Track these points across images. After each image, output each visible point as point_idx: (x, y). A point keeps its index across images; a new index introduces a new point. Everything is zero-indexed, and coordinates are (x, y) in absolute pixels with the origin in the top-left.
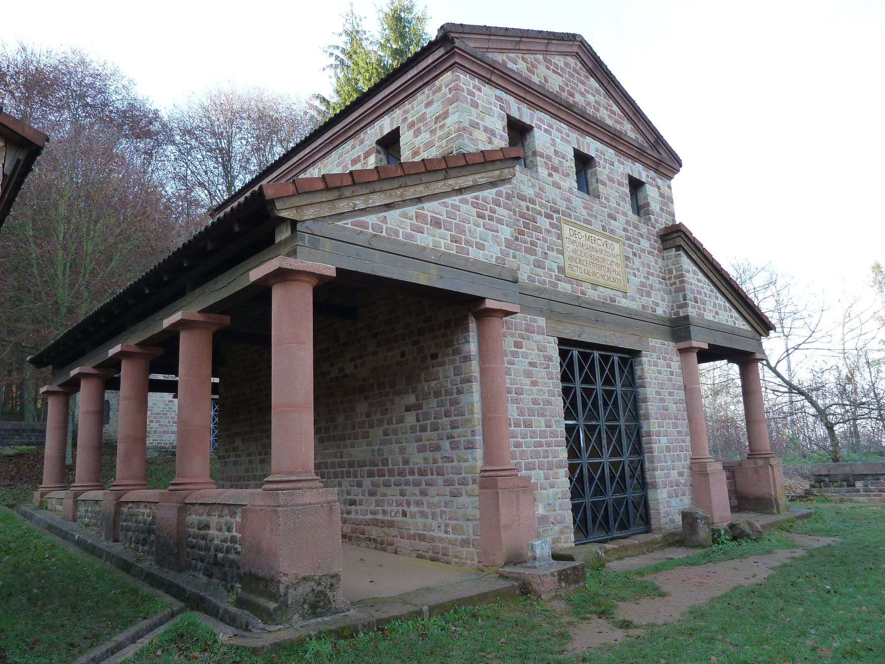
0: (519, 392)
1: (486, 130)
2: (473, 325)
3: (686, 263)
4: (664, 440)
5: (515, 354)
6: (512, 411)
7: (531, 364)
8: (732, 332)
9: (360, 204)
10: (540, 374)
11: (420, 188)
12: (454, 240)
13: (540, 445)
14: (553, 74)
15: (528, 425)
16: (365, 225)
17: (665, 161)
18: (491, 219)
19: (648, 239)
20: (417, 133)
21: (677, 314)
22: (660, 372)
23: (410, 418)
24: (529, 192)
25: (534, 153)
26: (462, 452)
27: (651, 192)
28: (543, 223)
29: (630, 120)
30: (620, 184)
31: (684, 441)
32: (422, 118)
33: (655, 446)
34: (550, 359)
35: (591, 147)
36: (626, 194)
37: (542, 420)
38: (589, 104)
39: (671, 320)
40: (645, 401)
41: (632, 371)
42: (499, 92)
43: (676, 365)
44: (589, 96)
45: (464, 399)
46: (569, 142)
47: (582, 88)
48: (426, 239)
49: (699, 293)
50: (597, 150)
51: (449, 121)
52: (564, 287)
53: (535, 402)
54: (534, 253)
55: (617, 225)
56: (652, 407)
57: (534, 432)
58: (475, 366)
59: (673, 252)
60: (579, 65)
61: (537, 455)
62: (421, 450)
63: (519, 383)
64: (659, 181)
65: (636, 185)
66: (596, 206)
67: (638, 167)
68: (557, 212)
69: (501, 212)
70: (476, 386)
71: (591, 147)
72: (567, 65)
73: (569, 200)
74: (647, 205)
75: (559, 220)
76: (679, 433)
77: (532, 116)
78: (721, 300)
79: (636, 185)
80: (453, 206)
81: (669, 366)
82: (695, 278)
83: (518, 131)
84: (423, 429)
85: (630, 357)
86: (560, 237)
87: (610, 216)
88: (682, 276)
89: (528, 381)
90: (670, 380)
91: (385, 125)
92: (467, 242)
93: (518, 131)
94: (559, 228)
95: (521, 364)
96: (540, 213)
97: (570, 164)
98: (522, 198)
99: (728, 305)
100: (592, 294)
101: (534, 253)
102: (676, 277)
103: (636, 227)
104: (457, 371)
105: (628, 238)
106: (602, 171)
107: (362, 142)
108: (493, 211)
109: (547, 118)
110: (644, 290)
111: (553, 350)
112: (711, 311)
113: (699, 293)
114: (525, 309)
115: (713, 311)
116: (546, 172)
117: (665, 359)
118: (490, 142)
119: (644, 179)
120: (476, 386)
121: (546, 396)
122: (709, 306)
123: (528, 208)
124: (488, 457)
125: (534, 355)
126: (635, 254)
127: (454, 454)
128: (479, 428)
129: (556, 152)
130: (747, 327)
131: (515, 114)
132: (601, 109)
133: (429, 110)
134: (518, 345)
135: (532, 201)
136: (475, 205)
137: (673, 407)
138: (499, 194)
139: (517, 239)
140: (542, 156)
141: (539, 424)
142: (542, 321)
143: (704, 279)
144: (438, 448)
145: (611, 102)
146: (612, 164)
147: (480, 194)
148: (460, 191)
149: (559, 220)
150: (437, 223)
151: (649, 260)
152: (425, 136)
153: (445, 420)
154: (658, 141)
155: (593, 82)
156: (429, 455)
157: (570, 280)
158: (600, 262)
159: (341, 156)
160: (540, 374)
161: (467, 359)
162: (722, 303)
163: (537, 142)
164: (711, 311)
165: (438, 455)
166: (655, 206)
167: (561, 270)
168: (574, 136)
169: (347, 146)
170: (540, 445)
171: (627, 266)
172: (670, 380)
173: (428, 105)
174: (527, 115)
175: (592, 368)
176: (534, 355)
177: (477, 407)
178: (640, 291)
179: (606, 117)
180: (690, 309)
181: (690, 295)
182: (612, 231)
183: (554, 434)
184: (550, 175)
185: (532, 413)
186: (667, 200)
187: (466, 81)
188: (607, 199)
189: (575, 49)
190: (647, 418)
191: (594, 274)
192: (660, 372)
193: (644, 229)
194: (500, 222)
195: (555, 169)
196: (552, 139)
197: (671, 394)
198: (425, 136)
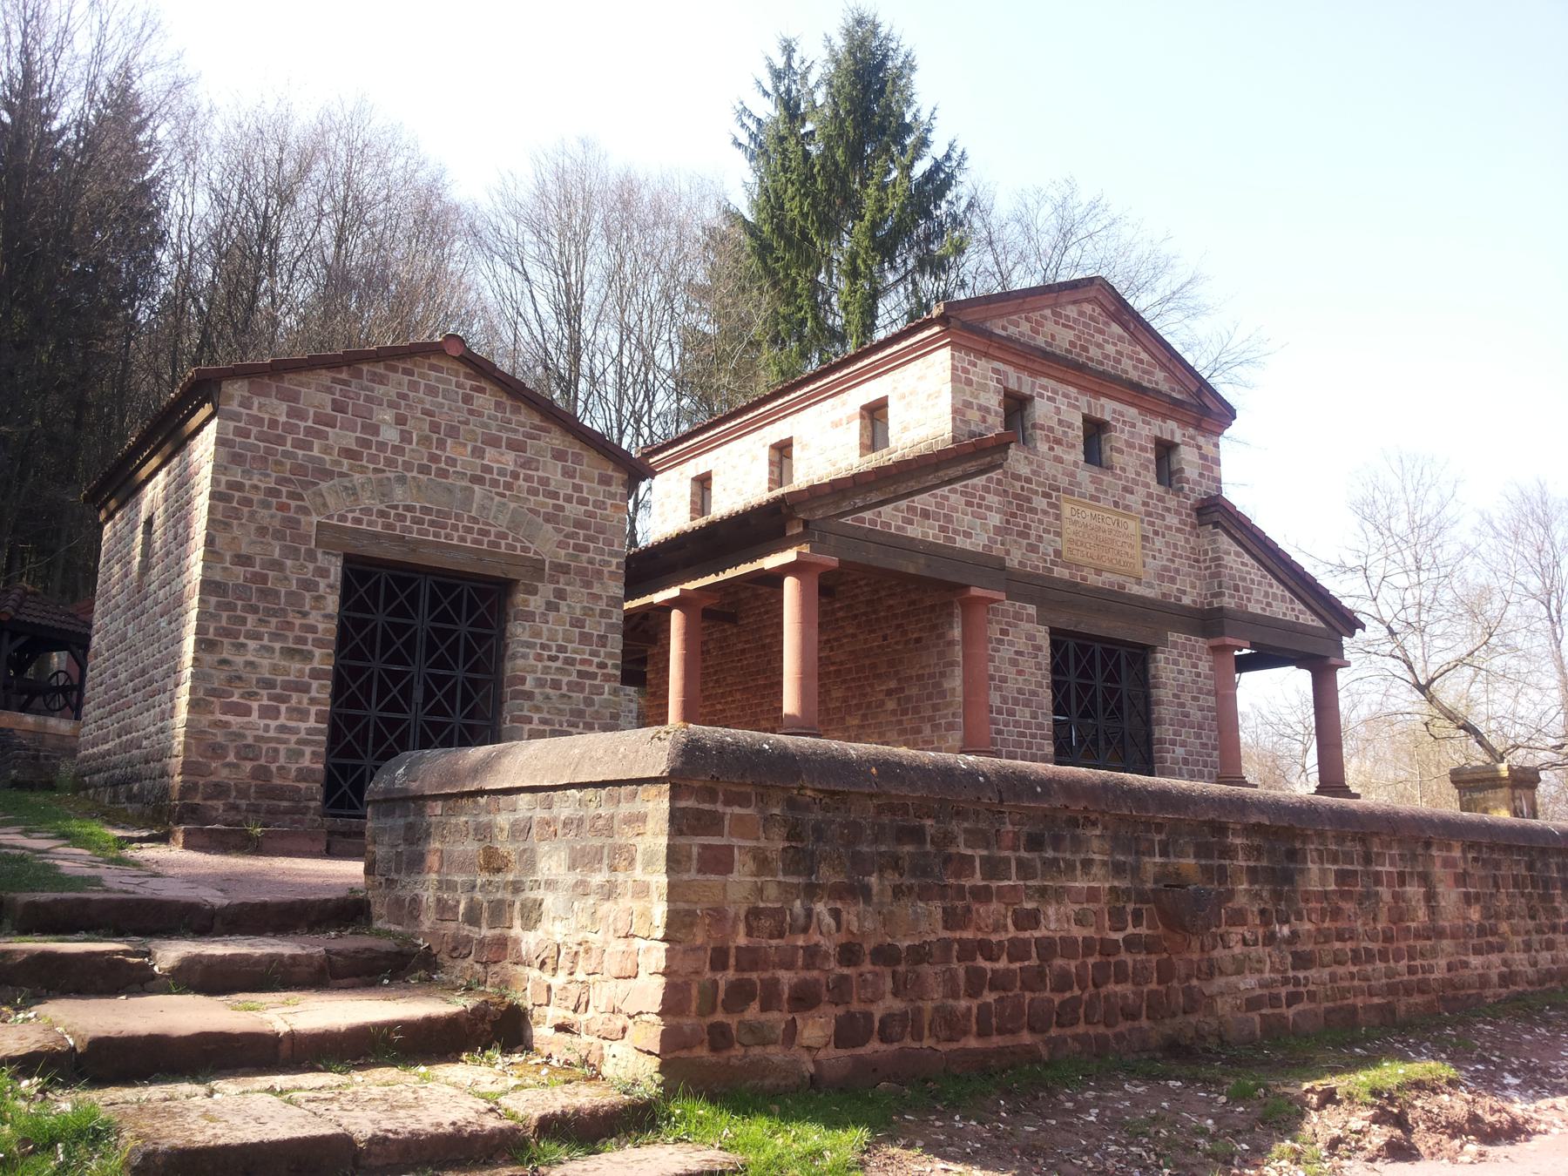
0: (1004, 680)
1: (980, 408)
2: (958, 611)
3: (1225, 542)
4: (1180, 751)
5: (1000, 641)
8: (1292, 628)
10: (1027, 664)
11: (912, 483)
12: (943, 529)
13: (1023, 735)
14: (1057, 334)
15: (1011, 713)
16: (863, 520)
17: (1206, 410)
18: (980, 506)
19: (1178, 513)
21: (1210, 603)
22: (1180, 672)
23: (891, 705)
24: (1025, 470)
27: (1187, 458)
28: (1040, 503)
29: (1163, 367)
31: (1209, 755)
34: (1039, 648)
35: (1107, 409)
36: (1149, 460)
37: (1027, 711)
38: (1107, 357)
41: (1145, 670)
43: (1204, 667)
44: (1110, 348)
46: (1077, 407)
47: (1099, 338)
48: (914, 531)
49: (1244, 579)
50: (1114, 411)
52: (1058, 572)
53: (1020, 691)
54: (1027, 536)
55: (1135, 500)
56: (1165, 711)
57: (1016, 721)
60: (1098, 310)
61: (1019, 744)
63: (1019, 654)
64: (1201, 440)
66: (1107, 478)
67: (1172, 424)
68: (1058, 490)
69: (992, 499)
70: (958, 671)
71: (1107, 409)
72: (1081, 314)
73: (1073, 475)
74: (1181, 470)
75: (1058, 498)
76: (1204, 745)
77: (1033, 384)
78: (1278, 589)
79: (1165, 450)
80: (943, 497)
81: (1195, 666)
82: (1237, 561)
83: (1016, 405)
84: (905, 712)
85: (1141, 655)
86: (1058, 517)
87: (1125, 489)
89: (1014, 670)
90: (1195, 682)
92: (956, 532)
93: (1016, 405)
94: (1056, 506)
95: (1006, 652)
96: (1036, 493)
98: (1017, 477)
99: (1287, 594)
100: (1093, 580)
101: (1027, 536)
102: (1212, 560)
103: (1161, 499)
104: (941, 655)
105: (1149, 514)
106: (1119, 436)
109: (1052, 383)
110: (1163, 575)
112: (1258, 601)
113: (1244, 579)
115: (1269, 600)
117: (1189, 657)
119: (1177, 439)
123: (1022, 488)
125: (1021, 644)
126: (1156, 533)
129: (1060, 422)
130: (1318, 623)
131: (1013, 385)
132: (1124, 360)
134: (1004, 632)
135: (1028, 480)
138: (989, 480)
139: (1008, 522)
140: (1042, 428)
141: (1024, 714)
142: (1032, 609)
145: (1138, 348)
146: (1133, 426)
147: (970, 482)
149: (1058, 498)
150: (926, 514)
154: (1203, 387)
155: (1116, 329)
158: (1110, 538)
160: (1027, 664)
161: (951, 643)
162: (1279, 592)
164: (1258, 601)
166: (1191, 472)
168: (1084, 401)
170: (1023, 735)
171: (1144, 547)
172: (1195, 682)
175: (1091, 660)
176: (1021, 644)
177: (959, 690)
178: (1161, 577)
179: (1130, 369)
180: (1226, 599)
182: (1127, 507)
183: (1040, 726)
184: (1051, 449)
185: (1016, 702)
186: (1211, 463)
188: (1123, 470)
189: (1092, 294)
190: (1160, 722)
192: (1180, 672)
193: (1172, 502)
194: (989, 508)
195: (1058, 442)
196: (1058, 408)
197: (1195, 699)
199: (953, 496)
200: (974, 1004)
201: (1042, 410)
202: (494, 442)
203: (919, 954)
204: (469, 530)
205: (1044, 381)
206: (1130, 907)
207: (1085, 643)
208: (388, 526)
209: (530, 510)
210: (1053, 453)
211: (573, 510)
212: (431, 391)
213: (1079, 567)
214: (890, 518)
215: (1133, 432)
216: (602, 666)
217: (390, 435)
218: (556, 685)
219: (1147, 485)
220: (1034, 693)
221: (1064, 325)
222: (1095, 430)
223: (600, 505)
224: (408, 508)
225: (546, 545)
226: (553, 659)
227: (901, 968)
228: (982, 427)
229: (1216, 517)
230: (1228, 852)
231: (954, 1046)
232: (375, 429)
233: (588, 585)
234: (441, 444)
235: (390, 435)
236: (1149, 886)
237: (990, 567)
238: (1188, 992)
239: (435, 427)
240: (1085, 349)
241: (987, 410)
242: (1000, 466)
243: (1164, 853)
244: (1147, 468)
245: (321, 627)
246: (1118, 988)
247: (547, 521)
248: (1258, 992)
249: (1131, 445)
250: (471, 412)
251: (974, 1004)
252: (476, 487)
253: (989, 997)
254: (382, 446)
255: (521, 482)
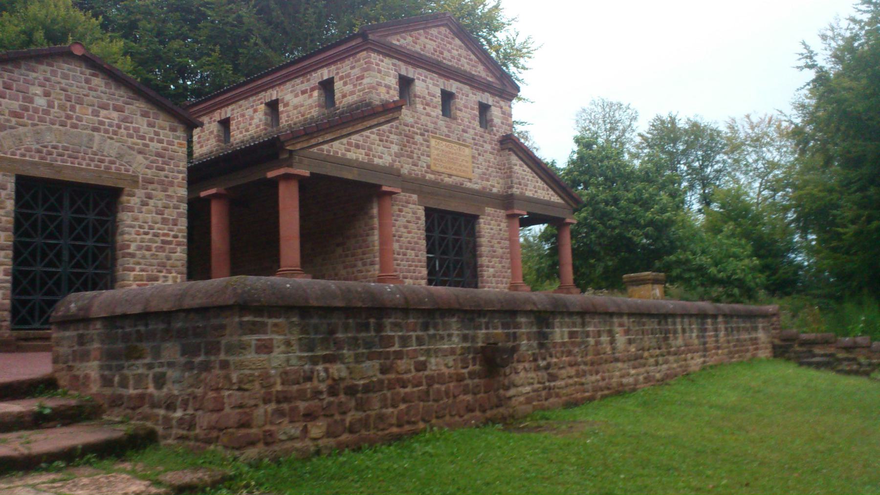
0: (400, 237)
3: (514, 159)
4: (491, 270)
5: (398, 216)
6: (396, 246)
7: (408, 222)
8: (548, 204)
9: (321, 140)
10: (412, 226)
15: (405, 254)
18: (387, 141)
19: (490, 143)
20: (345, 84)
24: (410, 120)
25: (415, 96)
26: (368, 267)
27: (495, 113)
28: (419, 139)
30: (472, 109)
32: (348, 75)
33: (485, 273)
34: (418, 218)
39: (502, 196)
40: (481, 246)
42: (395, 61)
43: (504, 225)
45: (370, 239)
46: (437, 86)
51: (365, 81)
52: (429, 176)
53: (409, 242)
56: (484, 250)
58: (376, 221)
59: (507, 152)
60: (448, 31)
62: (345, 268)
63: (404, 231)
64: (502, 103)
65: (484, 108)
68: (427, 131)
70: (376, 232)
71: (453, 86)
72: (439, 33)
73: (435, 123)
74: (492, 120)
76: (503, 267)
78: (540, 183)
79: (484, 108)
81: (499, 225)
82: (521, 169)
83: (405, 83)
84: (347, 256)
85: (472, 220)
86: (428, 147)
88: (510, 168)
89: (405, 230)
90: (499, 234)
91: (325, 74)
92: (374, 156)
93: (405, 83)
95: (402, 221)
96: (417, 134)
97: (438, 100)
100: (447, 180)
103: (482, 137)
105: (476, 144)
106: (460, 101)
107: (308, 80)
108: (388, 137)
110: (484, 177)
111: (421, 213)
113: (523, 179)
114: (404, 190)
116: (422, 107)
117: (496, 221)
118: (388, 93)
119: (490, 103)
120: (376, 232)
121: (416, 240)
122: (530, 187)
124: (382, 269)
126: (479, 154)
127: (363, 268)
128: (377, 254)
131: (403, 73)
132: (462, 59)
133: (353, 71)
134: (400, 210)
135: (412, 127)
136: (378, 135)
137: (500, 251)
138: (392, 127)
141: (411, 254)
142: (415, 197)
143: (528, 169)
144: (355, 266)
145: (470, 53)
146: (467, 96)
148: (370, 127)
151: (489, 157)
152: (349, 87)
153: (359, 251)
155: (457, 41)
156: (350, 270)
157: (433, 172)
159: (293, 86)
161: (372, 217)
163: (417, 88)
164: (531, 190)
165: (355, 269)
166: (497, 121)
167: (429, 167)
169: (298, 81)
171: (473, 162)
173: (352, 68)
174: (410, 72)
177: (377, 243)
180: (514, 190)
181: (516, 181)
182: (464, 140)
183: (420, 261)
184: (424, 109)
187: (374, 57)
188: (462, 120)
189: (446, 22)
191: (450, 168)
192: (492, 229)
193: (487, 136)
195: (428, 105)
196: (427, 86)
198: (349, 87)
199: (372, 135)
200: (396, 411)
201: (419, 87)
202: (105, 107)
203: (367, 389)
204: (92, 160)
205: (420, 70)
206: (470, 356)
207: (443, 214)
208: (42, 158)
209: (129, 147)
210: (424, 112)
211: (155, 146)
212: (65, 76)
213: (439, 173)
214: (337, 148)
215: (468, 100)
216: (175, 237)
217: (41, 102)
218: (149, 249)
219: (474, 129)
220: (416, 243)
221: (431, 39)
222: (447, 97)
223: (170, 143)
224: (55, 147)
225: (139, 165)
226: (146, 234)
227: (359, 395)
228: (387, 96)
229: (510, 146)
230: (517, 326)
231: (387, 432)
232: (31, 101)
233: (165, 190)
234: (73, 108)
235: (41, 102)
236: (480, 344)
237: (392, 173)
238: (498, 397)
239: (68, 99)
240: (442, 53)
241: (388, 87)
242: (397, 118)
243: (487, 328)
244: (474, 119)
245: (180, 235)
246: (465, 397)
247: (140, 153)
248: (532, 394)
249: (466, 107)
250: (90, 89)
251: (396, 411)
252: (95, 134)
253: (403, 406)
254: (36, 111)
255: (122, 130)
